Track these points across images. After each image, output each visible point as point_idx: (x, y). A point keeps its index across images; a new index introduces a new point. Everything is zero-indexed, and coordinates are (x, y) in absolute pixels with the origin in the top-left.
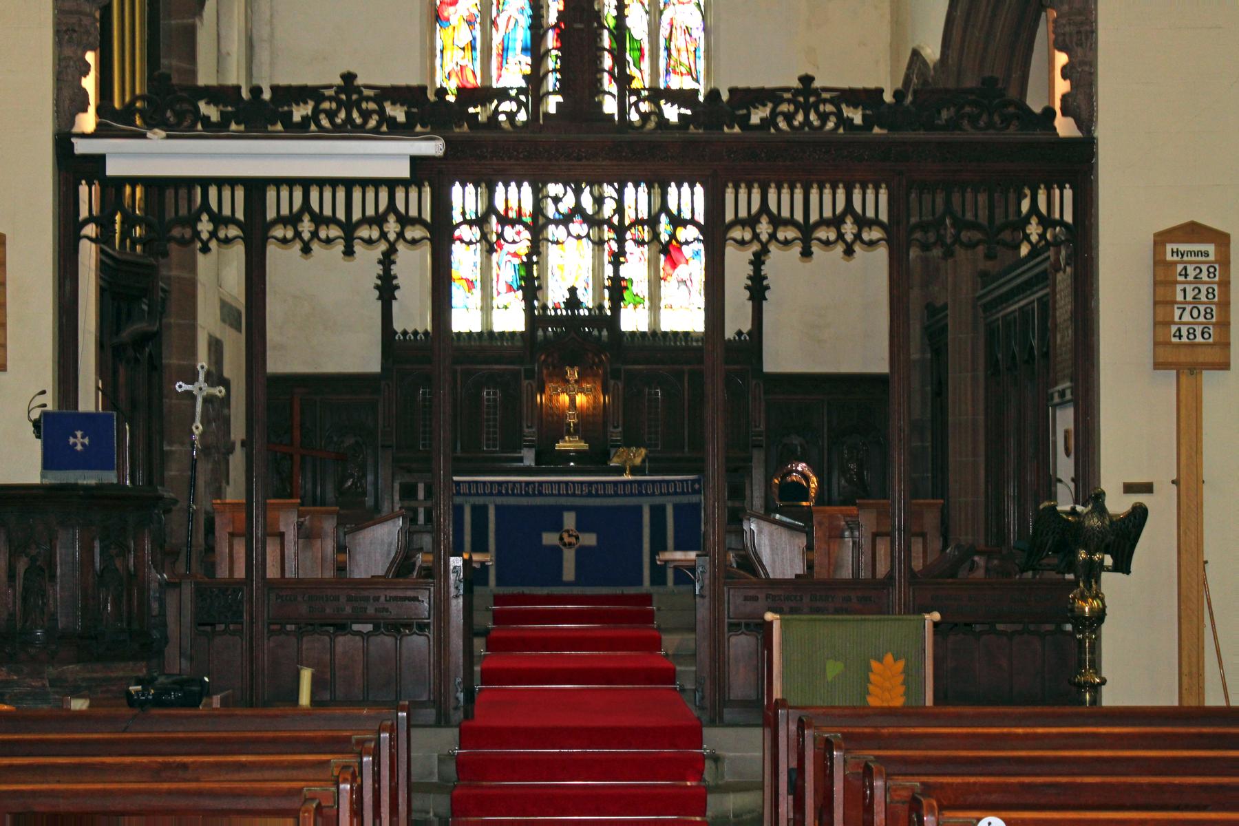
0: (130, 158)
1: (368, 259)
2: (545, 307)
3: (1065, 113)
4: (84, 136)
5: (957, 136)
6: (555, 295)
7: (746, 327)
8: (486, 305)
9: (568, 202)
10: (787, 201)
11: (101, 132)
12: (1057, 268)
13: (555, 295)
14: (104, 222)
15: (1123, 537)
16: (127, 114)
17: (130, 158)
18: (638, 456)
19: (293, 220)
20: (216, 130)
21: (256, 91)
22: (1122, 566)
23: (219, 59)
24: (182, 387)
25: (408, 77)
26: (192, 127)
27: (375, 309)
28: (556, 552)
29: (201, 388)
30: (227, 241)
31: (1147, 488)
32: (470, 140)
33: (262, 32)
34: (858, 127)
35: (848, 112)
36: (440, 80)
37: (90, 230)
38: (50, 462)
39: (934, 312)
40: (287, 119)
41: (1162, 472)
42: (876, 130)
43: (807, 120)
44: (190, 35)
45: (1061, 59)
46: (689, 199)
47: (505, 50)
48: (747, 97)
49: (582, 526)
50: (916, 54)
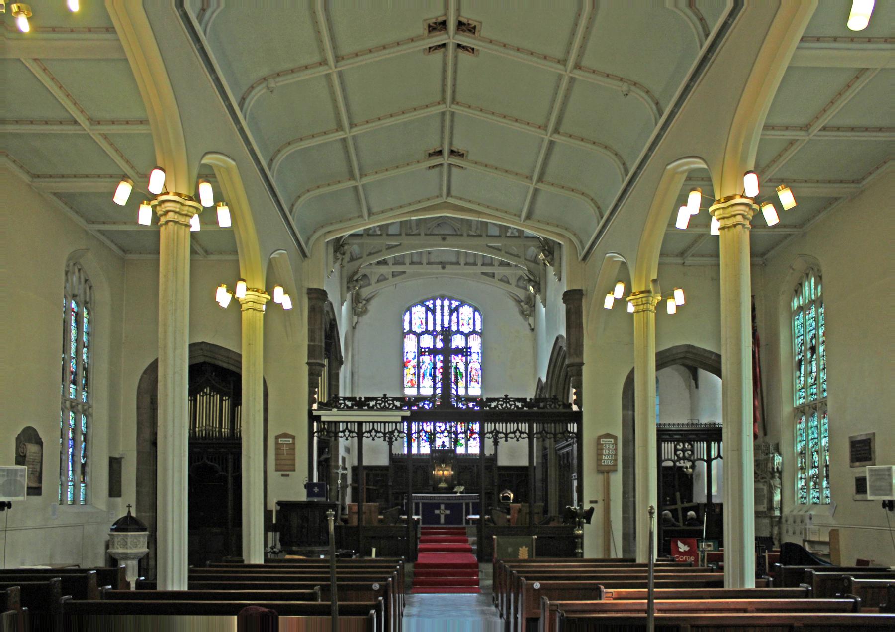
0: (327, 416)
5: (546, 410)
7: (493, 452)
9: (443, 428)
10: (501, 427)
11: (319, 409)
15: (588, 515)
17: (327, 416)
18: (462, 489)
22: (589, 522)
24: (335, 471)
29: (340, 471)
31: (596, 502)
32: (417, 411)
38: (309, 495)
39: (545, 448)
41: (600, 498)
44: (337, 375)
45: (574, 390)
47: (424, 375)
49: (446, 508)
50: (540, 379)
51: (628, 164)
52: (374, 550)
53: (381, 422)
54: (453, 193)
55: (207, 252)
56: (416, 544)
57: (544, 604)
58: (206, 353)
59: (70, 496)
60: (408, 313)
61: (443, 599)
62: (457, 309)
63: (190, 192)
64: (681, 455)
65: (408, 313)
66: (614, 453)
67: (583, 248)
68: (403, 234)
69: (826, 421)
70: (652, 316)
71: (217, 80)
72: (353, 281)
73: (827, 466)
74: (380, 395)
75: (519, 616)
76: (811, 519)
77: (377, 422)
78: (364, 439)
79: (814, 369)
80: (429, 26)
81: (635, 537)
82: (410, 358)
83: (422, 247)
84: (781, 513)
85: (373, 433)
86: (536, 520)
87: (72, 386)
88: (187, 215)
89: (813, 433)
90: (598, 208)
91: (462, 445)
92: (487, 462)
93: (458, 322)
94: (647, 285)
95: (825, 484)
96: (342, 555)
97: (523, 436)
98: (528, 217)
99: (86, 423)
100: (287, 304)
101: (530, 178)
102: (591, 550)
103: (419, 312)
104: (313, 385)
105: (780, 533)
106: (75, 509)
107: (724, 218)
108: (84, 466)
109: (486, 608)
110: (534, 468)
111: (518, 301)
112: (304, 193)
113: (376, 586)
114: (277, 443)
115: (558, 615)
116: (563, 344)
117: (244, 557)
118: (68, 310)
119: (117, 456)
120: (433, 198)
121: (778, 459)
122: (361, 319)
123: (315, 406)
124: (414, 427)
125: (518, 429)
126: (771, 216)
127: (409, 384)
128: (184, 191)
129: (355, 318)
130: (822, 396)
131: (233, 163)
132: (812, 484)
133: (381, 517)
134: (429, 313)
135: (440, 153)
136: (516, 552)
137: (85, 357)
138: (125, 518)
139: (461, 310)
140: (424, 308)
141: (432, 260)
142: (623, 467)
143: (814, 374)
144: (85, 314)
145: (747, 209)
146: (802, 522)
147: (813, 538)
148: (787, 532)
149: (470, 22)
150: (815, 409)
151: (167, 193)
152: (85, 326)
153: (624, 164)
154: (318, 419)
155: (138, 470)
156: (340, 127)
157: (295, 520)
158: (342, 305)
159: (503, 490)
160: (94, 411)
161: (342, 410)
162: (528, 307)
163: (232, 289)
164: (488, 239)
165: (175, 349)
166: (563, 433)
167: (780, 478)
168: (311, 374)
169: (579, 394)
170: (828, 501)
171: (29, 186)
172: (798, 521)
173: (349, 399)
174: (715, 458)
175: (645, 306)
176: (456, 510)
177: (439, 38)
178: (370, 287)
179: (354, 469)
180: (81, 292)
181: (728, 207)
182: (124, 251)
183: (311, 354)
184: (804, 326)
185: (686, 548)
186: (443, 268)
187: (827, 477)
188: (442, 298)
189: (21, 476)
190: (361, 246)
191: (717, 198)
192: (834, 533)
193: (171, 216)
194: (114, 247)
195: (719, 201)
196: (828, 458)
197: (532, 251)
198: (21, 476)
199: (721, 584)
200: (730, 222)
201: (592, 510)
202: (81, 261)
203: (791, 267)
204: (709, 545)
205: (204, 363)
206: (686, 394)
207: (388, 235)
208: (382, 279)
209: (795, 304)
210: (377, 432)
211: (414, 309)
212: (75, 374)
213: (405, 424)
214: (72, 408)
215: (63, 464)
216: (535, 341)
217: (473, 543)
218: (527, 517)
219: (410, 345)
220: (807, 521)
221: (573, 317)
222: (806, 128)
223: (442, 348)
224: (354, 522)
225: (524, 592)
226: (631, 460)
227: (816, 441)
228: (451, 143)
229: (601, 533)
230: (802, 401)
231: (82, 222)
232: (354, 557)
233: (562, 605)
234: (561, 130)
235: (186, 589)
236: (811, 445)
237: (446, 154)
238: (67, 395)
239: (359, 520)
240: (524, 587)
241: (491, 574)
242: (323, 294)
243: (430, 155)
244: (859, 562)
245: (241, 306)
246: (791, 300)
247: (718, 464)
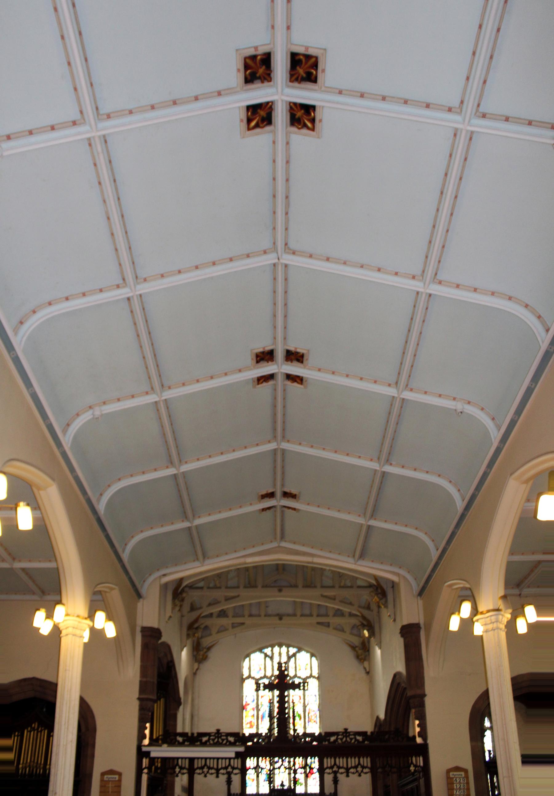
1: (223, 778)
2: (274, 786)
3: (419, 736)
4: (145, 746)
10: (341, 761)
12: (420, 778)
14: (149, 768)
16: (157, 740)
19: (202, 768)
20: (181, 744)
21: (193, 734)
23: (183, 724)
25: (236, 730)
26: (175, 743)
27: (225, 788)
30: (183, 774)
34: (361, 742)
37: (146, 771)
40: (201, 741)
42: (366, 742)
43: (346, 740)
45: (417, 722)
46: (315, 763)
48: (329, 734)
53: (214, 758)
62: (294, 655)
77: (210, 758)
78: (196, 775)
80: (257, 356)
91: (301, 784)
100: (111, 631)
111: (353, 648)
114: (102, 780)
123: (146, 742)
124: (251, 762)
127: (249, 725)
129: (196, 665)
135: (271, 495)
140: (263, 655)
141: (270, 612)
149: (298, 350)
154: (147, 754)
158: (182, 650)
162: (363, 652)
175: (495, 625)
177: (266, 369)
188: (280, 646)
208: (222, 630)
210: (209, 768)
213: (240, 760)
219: (249, 687)
228: (283, 485)
243: (264, 497)
245: (61, 632)
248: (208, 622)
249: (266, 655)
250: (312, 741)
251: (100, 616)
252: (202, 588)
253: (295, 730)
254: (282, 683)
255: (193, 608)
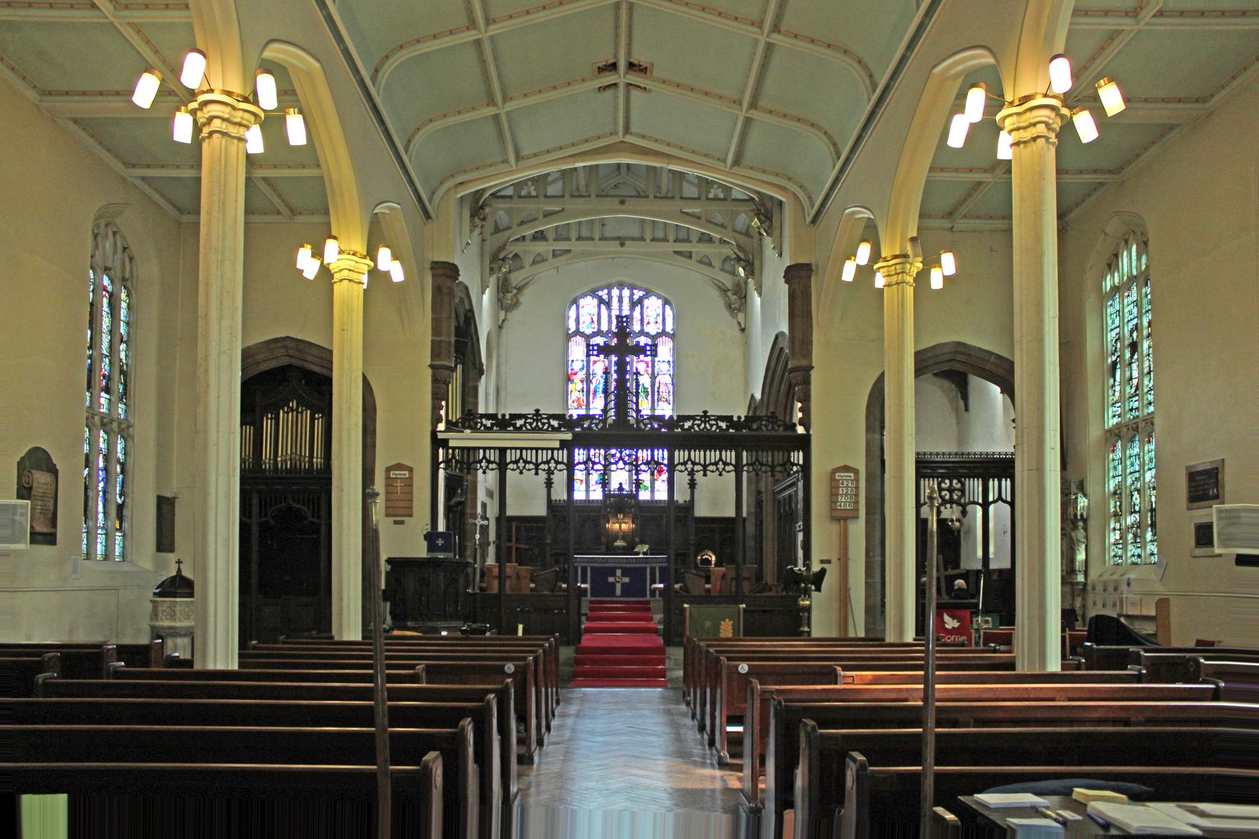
1: (543, 476)
6: (614, 486)
7: (688, 499)
8: (588, 490)
10: (697, 455)
11: (448, 430)
13: (614, 486)
15: (818, 579)
18: (646, 548)
22: (818, 589)
28: (613, 585)
29: (479, 522)
31: (829, 562)
32: (584, 434)
33: (502, 385)
35: (720, 424)
36: (571, 412)
38: (430, 549)
39: (759, 493)
41: (834, 557)
45: (799, 405)
47: (595, 392)
49: (624, 575)
50: (752, 396)
51: (876, 76)
52: (521, 627)
53: (532, 449)
54: (633, 129)
55: (293, 212)
56: (580, 622)
57: (752, 690)
58: (291, 352)
59: (100, 549)
60: (574, 307)
61: (616, 694)
62: (640, 301)
63: (245, 89)
64: (947, 497)
65: (574, 307)
66: (854, 493)
67: (812, 206)
68: (567, 196)
69: (1152, 447)
70: (910, 291)
71: (329, 19)
72: (497, 259)
73: (1152, 510)
74: (530, 411)
75: (717, 713)
76: (1129, 584)
77: (527, 449)
79: (1135, 374)
81: (883, 613)
82: (576, 369)
83: (591, 213)
84: (1086, 577)
85: (521, 464)
86: (746, 586)
87: (103, 394)
88: (240, 124)
89: (1132, 465)
90: (834, 144)
91: (646, 488)
92: (679, 513)
93: (642, 320)
94: (903, 247)
95: (1149, 536)
96: (474, 631)
97: (727, 468)
98: (737, 162)
99: (125, 448)
100: (398, 275)
101: (739, 102)
102: (821, 624)
103: (588, 305)
104: (439, 395)
105: (1084, 607)
106: (108, 566)
107: (1018, 129)
108: (120, 508)
109: (673, 706)
110: (744, 520)
111: (724, 291)
112: (424, 124)
113: (510, 668)
114: (388, 478)
115: (772, 703)
116: (785, 344)
117: (334, 633)
118: (98, 288)
119: (169, 495)
120: (605, 136)
121: (1082, 502)
122: (510, 315)
123: (441, 427)
124: (580, 455)
125: (721, 459)
126: (1086, 127)
128: (237, 88)
129: (502, 314)
130: (1146, 411)
131: (317, 65)
132: (1130, 536)
133: (533, 585)
134: (603, 307)
135: (613, 67)
136: (716, 628)
137: (123, 355)
138: (174, 577)
139: (646, 302)
140: (595, 301)
141: (607, 234)
142: (867, 514)
143: (1135, 382)
144: (123, 296)
145: (1053, 115)
146: (1116, 589)
147: (1136, 612)
148: (1094, 604)
150: (1136, 429)
151: (212, 91)
152: (123, 312)
153: (871, 76)
155: (330, 605)
156: (472, 25)
157: (411, 584)
158: (483, 293)
159: (702, 550)
160: (136, 431)
161: (478, 431)
162: (737, 300)
163: (318, 253)
164: (683, 202)
165: (221, 318)
166: (783, 465)
167: (1085, 529)
168: (435, 380)
169: (806, 410)
170: (1154, 559)
171: (37, 106)
172: (1111, 589)
173: (488, 417)
174: (994, 502)
175: (900, 277)
176: (637, 576)
178: (522, 271)
179: (498, 520)
180: (118, 264)
181: (1025, 112)
182: (179, 210)
183: (435, 354)
184: (1122, 315)
185: (956, 624)
186: (622, 245)
187: (1153, 525)
188: (621, 286)
189: (22, 515)
190: (509, 212)
191: (1009, 98)
192: (1163, 604)
193: (217, 124)
194: (163, 203)
195: (1011, 103)
196: (1153, 499)
197: (742, 220)
198: (22, 515)
199: (1011, 665)
200: (1026, 135)
201: (823, 572)
202: (118, 221)
203: (1103, 231)
204: (987, 622)
205: (289, 366)
206: (953, 420)
207: (546, 196)
208: (539, 260)
209: (1108, 284)
210: (526, 462)
211: (582, 302)
212: (109, 378)
214: (104, 425)
215: (90, 503)
216: (747, 344)
217: (659, 623)
218: (734, 583)
219: (577, 350)
220: (1124, 587)
221: (798, 302)
222: (1134, 13)
223: (620, 352)
224: (495, 588)
225: (724, 685)
226: (878, 504)
227: (1137, 475)
228: (629, 53)
229: (836, 605)
230: (1116, 420)
231: (119, 167)
232: (488, 634)
233: (779, 692)
234: (783, 29)
235: (236, 667)
236: (1129, 481)
237: (623, 70)
238: (95, 406)
239: (501, 585)
240: (724, 673)
241: (682, 662)
242: (452, 270)
243: (601, 70)
244: (1199, 642)
245: (332, 276)
246: (1103, 277)
247: (995, 509)
248: (518, 248)
249: (601, 301)
250: (660, 427)
251: (384, 254)
252: (511, 197)
253: (638, 411)
254: (622, 345)
255: (497, 230)
